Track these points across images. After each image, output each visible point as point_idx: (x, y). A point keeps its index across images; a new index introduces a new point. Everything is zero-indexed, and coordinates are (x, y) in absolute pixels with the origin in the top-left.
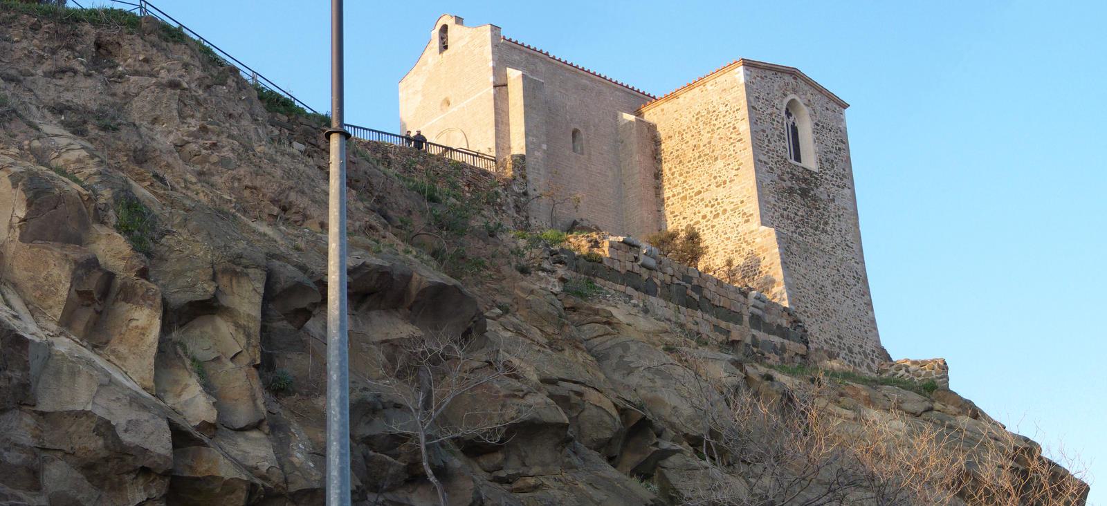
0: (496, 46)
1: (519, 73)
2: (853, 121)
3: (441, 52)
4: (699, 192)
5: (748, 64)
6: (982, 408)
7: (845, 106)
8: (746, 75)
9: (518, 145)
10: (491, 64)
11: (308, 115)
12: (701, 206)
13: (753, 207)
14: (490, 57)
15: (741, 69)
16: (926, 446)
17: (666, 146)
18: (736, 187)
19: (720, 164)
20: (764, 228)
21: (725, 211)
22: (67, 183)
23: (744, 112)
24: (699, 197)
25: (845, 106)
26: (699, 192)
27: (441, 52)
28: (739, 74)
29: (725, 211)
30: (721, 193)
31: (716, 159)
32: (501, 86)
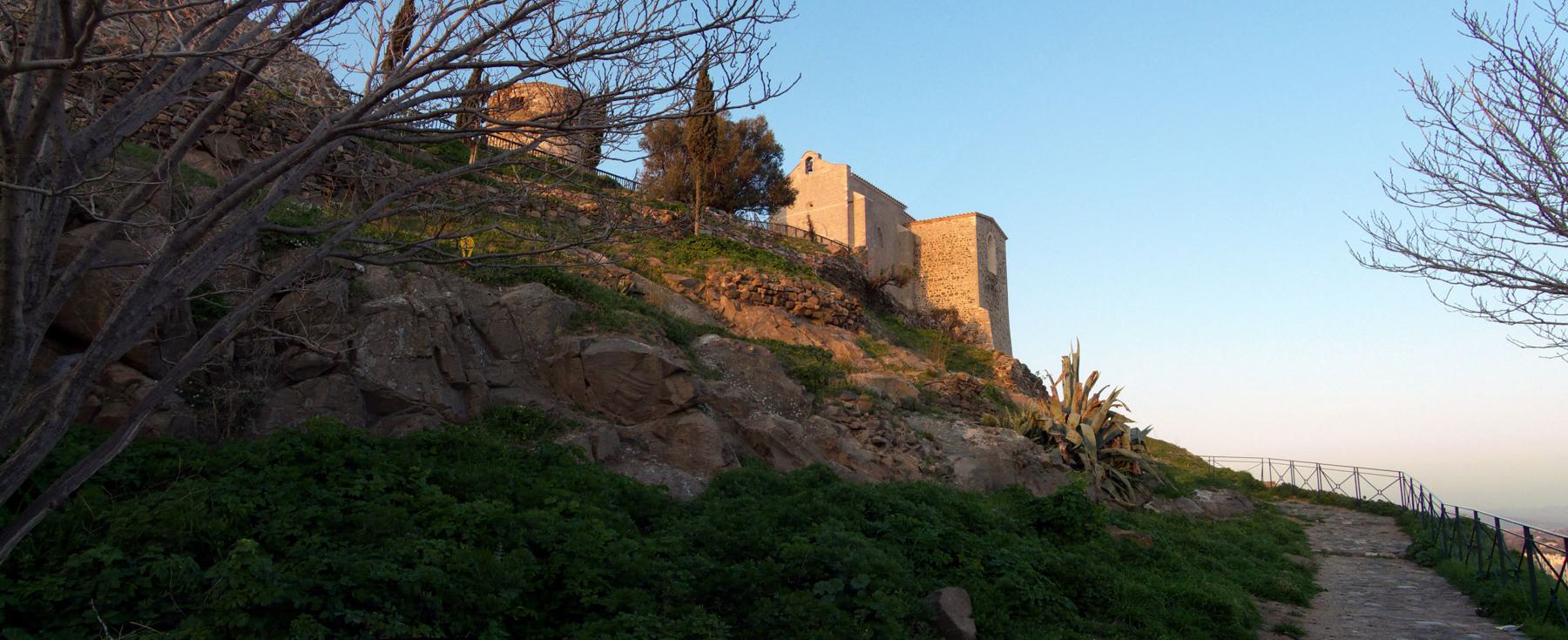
0: (849, 178)
1: (863, 197)
2: (1009, 246)
3: (807, 173)
4: (941, 279)
5: (979, 216)
6: (1174, 443)
7: (1006, 238)
8: (977, 221)
9: (599, 174)
10: (846, 189)
11: (513, 154)
12: (941, 287)
13: (975, 295)
14: (846, 184)
15: (975, 217)
16: (1223, 495)
17: (923, 248)
18: (965, 282)
19: (956, 266)
20: (980, 308)
21: (957, 294)
22: (1296, 503)
23: (974, 241)
24: (941, 282)
25: (1006, 238)
26: (941, 279)
27: (807, 173)
28: (974, 220)
29: (957, 294)
30: (955, 283)
31: (954, 263)
32: (851, 202)
